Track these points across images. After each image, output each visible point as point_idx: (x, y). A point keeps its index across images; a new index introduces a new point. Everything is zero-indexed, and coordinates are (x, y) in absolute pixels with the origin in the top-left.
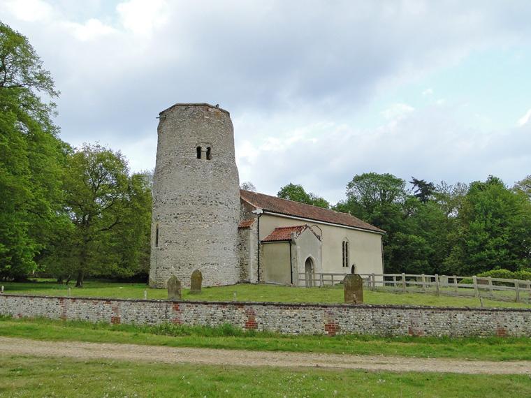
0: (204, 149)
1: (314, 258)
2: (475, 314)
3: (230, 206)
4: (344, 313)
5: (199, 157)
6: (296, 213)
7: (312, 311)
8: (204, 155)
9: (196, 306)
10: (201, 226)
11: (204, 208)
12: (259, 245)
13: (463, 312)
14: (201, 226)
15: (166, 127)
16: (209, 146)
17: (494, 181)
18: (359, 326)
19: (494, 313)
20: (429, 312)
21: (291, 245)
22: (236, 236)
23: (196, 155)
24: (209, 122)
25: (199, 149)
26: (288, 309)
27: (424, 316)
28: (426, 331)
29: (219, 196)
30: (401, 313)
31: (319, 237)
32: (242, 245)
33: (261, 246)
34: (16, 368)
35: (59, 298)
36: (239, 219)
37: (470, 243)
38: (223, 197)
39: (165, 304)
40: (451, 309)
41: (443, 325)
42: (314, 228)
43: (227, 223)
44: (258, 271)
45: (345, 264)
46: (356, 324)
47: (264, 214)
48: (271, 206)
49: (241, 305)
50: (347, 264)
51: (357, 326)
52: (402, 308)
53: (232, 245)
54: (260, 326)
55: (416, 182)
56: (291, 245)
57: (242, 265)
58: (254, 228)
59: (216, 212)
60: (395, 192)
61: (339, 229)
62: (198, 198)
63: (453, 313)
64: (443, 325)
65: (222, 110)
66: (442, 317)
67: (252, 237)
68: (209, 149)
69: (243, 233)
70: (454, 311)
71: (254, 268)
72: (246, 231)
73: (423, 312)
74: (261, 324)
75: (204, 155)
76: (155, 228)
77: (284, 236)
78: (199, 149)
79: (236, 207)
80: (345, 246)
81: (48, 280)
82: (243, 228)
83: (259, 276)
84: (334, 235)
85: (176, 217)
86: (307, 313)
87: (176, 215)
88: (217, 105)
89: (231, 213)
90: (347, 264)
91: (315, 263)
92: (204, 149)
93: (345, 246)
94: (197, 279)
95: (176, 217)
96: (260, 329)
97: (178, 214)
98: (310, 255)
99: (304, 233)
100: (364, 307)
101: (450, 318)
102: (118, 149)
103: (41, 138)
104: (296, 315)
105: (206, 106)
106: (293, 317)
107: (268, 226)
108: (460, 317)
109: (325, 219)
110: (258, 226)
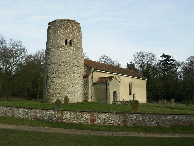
0: (69, 41)
1: (117, 91)
2: (182, 116)
3: (80, 67)
4: (131, 116)
5: (66, 44)
7: (118, 115)
8: (68, 43)
9: (70, 112)
11: (68, 68)
12: (92, 85)
13: (177, 115)
15: (52, 30)
16: (71, 39)
18: (137, 121)
19: (189, 116)
20: (164, 115)
21: (107, 85)
22: (83, 81)
24: (71, 28)
25: (66, 41)
26: (108, 114)
27: (162, 117)
28: (163, 123)
29: (75, 63)
30: (153, 116)
31: (119, 82)
32: (85, 85)
33: (93, 85)
36: (83, 73)
38: (76, 63)
39: (56, 111)
40: (173, 114)
41: (169, 121)
42: (117, 77)
44: (92, 96)
45: (130, 93)
46: (136, 121)
47: (95, 71)
48: (99, 66)
50: (131, 94)
51: (136, 121)
52: (154, 114)
54: (96, 121)
56: (107, 85)
57: (84, 93)
58: (90, 77)
59: (73, 70)
60: (152, 60)
61: (130, 78)
62: (66, 63)
64: (169, 121)
65: (76, 23)
66: (169, 117)
67: (90, 81)
68: (71, 41)
70: (174, 115)
71: (90, 95)
72: (87, 78)
73: (162, 115)
74: (97, 120)
75: (68, 43)
76: (46, 76)
77: (104, 81)
78: (66, 41)
79: (82, 67)
81: (143, 135)
82: (86, 77)
83: (92, 99)
84: (126, 80)
85: (56, 72)
87: (56, 71)
88: (75, 20)
89: (80, 70)
90: (131, 94)
91: (117, 94)
92: (69, 41)
94: (66, 99)
95: (56, 72)
97: (57, 70)
98: (115, 90)
99: (113, 80)
100: (139, 114)
101: (172, 118)
102: (127, 64)
104: (111, 117)
105: (69, 20)
106: (110, 118)
107: (97, 75)
108: (176, 117)
109: (104, 70)
110: (92, 76)
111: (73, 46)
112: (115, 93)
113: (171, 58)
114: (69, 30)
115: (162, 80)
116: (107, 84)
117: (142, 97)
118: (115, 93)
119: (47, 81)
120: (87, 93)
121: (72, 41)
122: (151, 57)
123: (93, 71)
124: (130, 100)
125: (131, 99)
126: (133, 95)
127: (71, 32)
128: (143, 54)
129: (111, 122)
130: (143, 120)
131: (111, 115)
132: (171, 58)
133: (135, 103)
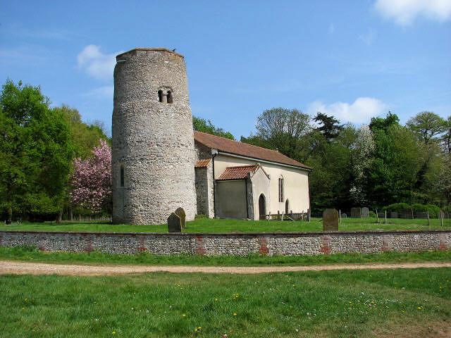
0: (165, 92)
5: (161, 100)
6: (244, 153)
8: (165, 98)
10: (166, 167)
14: (166, 167)
16: (169, 89)
17: (76, 111)
23: (158, 99)
31: (268, 176)
34: (22, 294)
35: (82, 234)
37: (374, 176)
43: (188, 163)
45: (281, 199)
49: (255, 236)
53: (191, 184)
55: (320, 117)
63: (411, 235)
66: (403, 238)
67: (209, 176)
69: (199, 172)
72: (203, 170)
75: (165, 98)
77: (240, 175)
80: (281, 181)
86: (308, 240)
93: (281, 181)
96: (271, 253)
103: (363, 96)
108: (416, 237)
111: (175, 103)
112: (262, 198)
113: (335, 124)
114: (165, 70)
115: (364, 178)
116: (247, 180)
117: (300, 202)
118: (262, 198)
119: (122, 179)
120: (206, 201)
121: (172, 94)
122: (298, 118)
123: (216, 154)
124: (293, 212)
125: (282, 211)
126: (285, 201)
127: (170, 75)
128: (279, 113)
129: (299, 252)
130: (358, 244)
131: (298, 239)
132: (335, 124)
133: (289, 216)
